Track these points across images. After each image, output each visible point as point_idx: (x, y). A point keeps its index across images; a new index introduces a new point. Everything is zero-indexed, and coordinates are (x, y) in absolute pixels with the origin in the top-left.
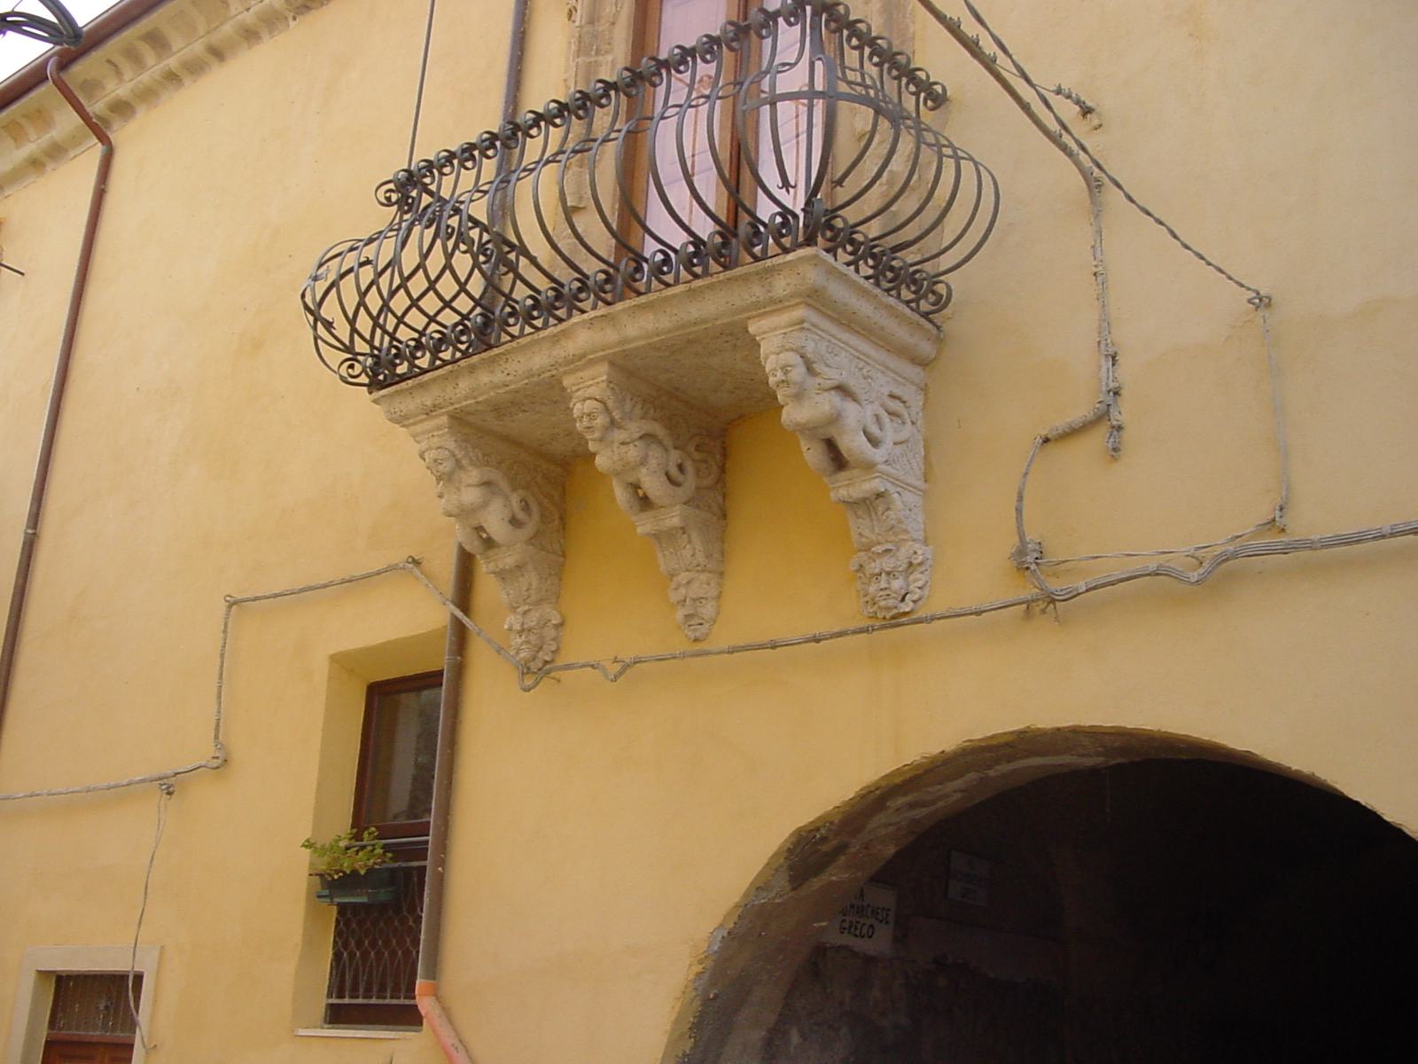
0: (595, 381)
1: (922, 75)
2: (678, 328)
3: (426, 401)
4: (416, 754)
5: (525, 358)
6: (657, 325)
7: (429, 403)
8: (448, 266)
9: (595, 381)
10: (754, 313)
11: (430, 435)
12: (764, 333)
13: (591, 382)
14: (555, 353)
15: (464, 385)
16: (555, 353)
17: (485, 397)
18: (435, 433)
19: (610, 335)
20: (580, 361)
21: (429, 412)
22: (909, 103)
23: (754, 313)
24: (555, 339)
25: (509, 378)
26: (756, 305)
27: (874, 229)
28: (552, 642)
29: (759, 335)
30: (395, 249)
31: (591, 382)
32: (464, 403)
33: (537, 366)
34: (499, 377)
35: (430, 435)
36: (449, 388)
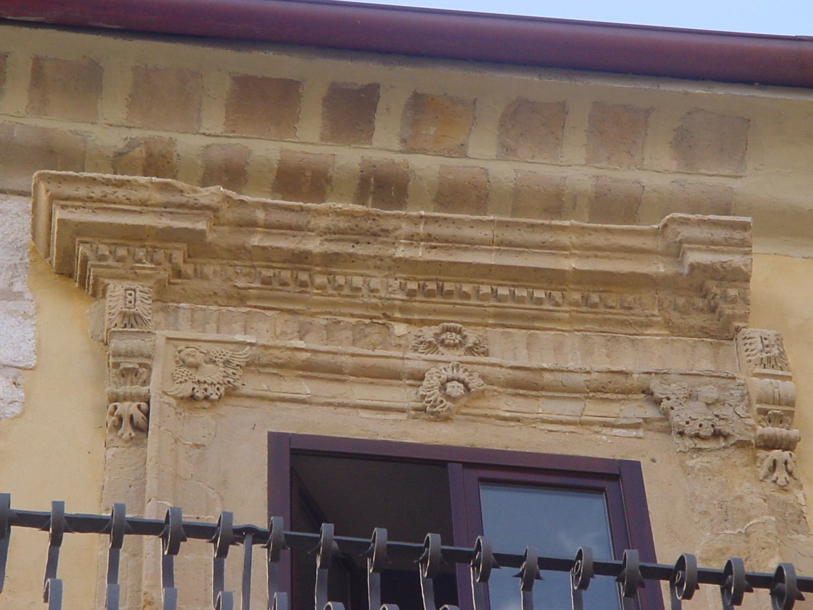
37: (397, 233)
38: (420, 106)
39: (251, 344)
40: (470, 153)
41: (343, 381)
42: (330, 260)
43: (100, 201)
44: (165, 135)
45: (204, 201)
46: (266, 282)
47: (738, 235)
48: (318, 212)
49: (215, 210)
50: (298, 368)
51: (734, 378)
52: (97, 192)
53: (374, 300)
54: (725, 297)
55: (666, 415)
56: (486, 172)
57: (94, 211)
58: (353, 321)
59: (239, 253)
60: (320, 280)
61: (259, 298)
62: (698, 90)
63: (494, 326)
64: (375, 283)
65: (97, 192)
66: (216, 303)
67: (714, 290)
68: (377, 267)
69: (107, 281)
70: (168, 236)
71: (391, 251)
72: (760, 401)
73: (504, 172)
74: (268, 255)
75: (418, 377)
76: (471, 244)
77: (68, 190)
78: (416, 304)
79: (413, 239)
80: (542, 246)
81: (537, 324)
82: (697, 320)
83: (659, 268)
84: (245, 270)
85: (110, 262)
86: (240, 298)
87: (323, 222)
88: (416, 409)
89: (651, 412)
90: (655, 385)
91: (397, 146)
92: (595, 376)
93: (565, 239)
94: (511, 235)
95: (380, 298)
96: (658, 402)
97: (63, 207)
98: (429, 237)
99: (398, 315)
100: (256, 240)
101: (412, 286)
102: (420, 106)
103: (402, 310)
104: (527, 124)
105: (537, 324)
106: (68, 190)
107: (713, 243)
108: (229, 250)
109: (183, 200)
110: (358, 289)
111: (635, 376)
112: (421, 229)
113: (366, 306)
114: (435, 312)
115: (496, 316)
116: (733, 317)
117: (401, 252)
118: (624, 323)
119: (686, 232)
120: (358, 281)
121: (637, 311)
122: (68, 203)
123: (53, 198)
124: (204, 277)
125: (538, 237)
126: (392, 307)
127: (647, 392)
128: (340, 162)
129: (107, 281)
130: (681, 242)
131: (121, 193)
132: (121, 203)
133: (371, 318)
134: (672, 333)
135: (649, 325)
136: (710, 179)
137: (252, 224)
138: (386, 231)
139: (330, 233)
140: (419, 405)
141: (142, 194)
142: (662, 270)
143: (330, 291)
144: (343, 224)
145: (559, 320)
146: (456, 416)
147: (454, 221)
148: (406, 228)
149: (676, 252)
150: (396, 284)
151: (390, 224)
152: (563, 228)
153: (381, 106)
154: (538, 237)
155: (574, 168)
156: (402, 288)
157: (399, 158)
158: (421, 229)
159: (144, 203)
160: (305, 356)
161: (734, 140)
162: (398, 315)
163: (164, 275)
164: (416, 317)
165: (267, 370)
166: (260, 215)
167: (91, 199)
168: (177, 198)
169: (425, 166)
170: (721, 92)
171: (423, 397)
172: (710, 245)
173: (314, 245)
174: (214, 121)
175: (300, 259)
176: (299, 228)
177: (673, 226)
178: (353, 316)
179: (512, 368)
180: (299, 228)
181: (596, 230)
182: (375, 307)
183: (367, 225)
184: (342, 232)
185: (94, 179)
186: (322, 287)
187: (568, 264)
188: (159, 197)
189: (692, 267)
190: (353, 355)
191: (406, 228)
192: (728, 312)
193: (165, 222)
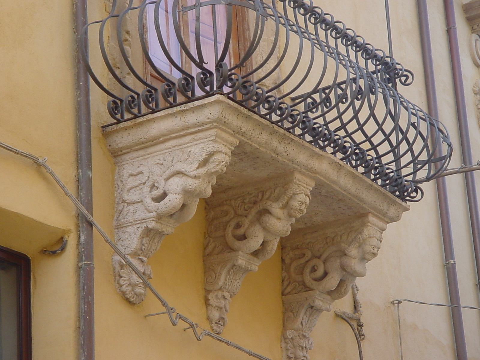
0: (307, 187)
1: (328, 18)
2: (354, 196)
3: (244, 127)
4: (78, 261)
5: (297, 153)
6: (351, 188)
7: (244, 129)
8: (372, 115)
9: (307, 187)
10: (375, 213)
11: (225, 144)
12: (373, 224)
13: (305, 186)
14: (310, 161)
15: (265, 137)
16: (310, 161)
17: (264, 150)
18: (228, 145)
19: (332, 174)
20: (310, 172)
21: (236, 132)
22: (342, 49)
23: (375, 213)
24: (313, 155)
25: (284, 154)
26: (380, 211)
27: (269, 82)
28: (289, 348)
29: (371, 224)
30: (428, 129)
31: (305, 186)
33: (299, 160)
34: (281, 148)
35: (225, 144)
36: (258, 132)
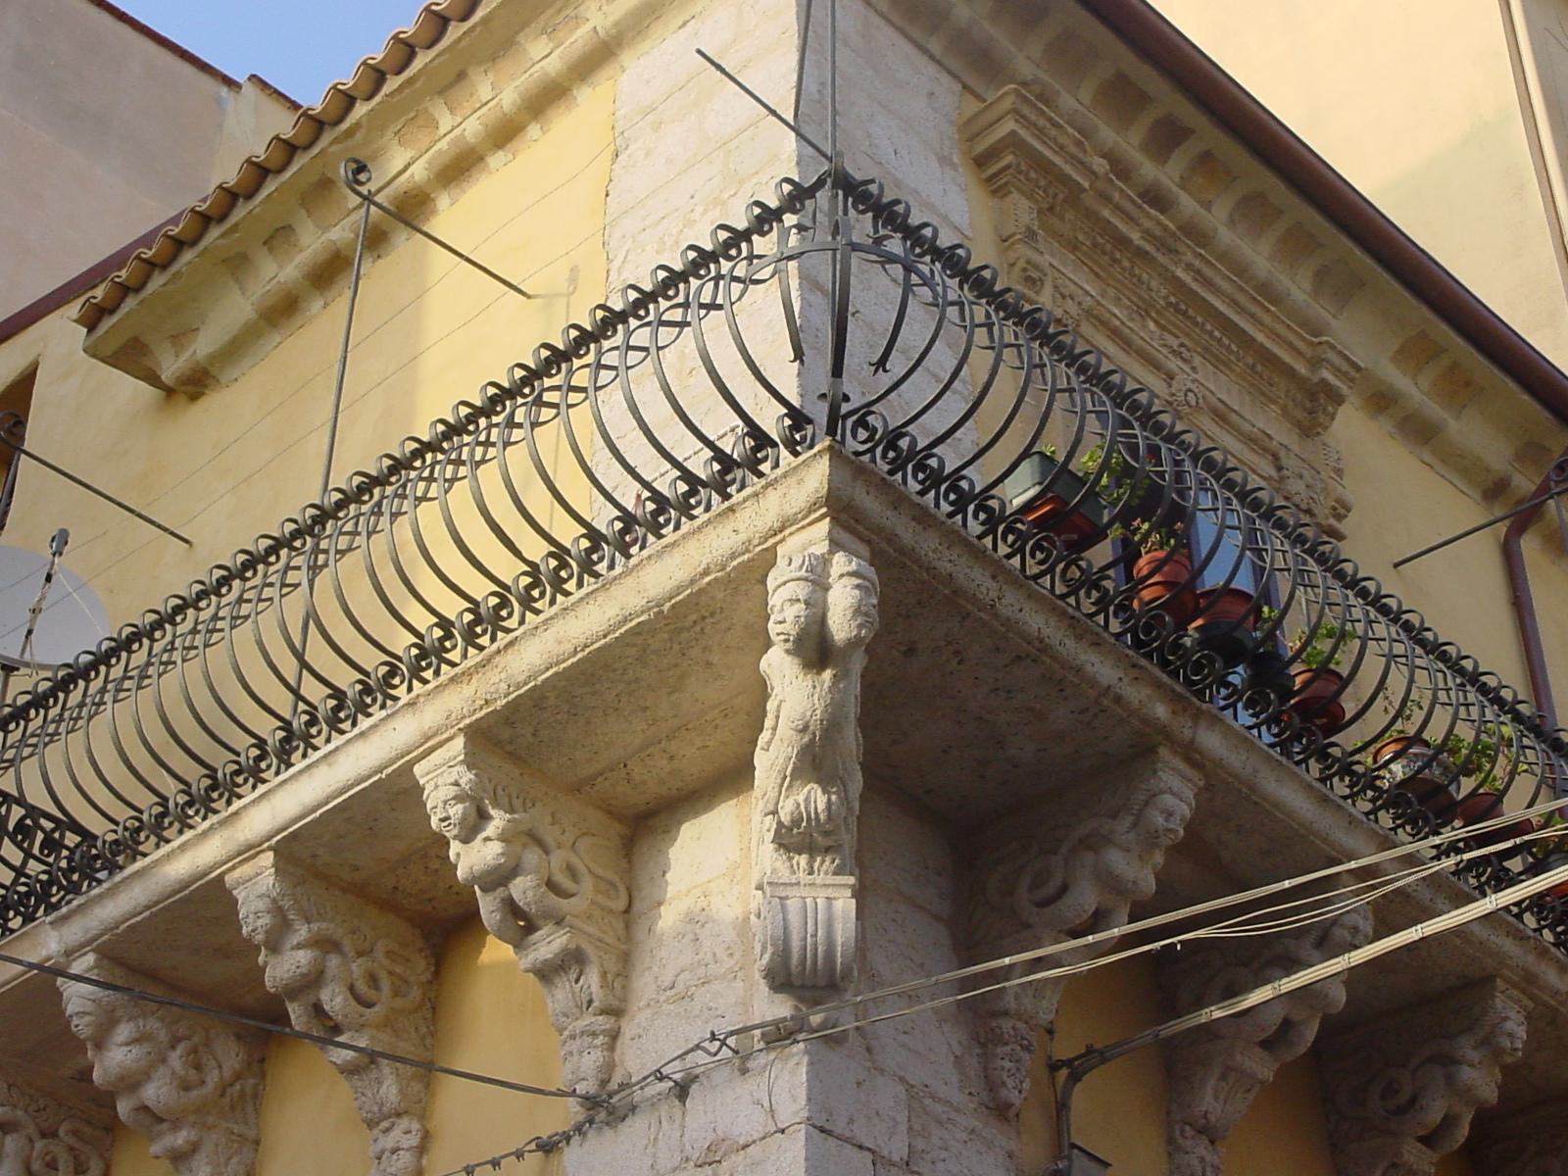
32: (1317, 842)
35: (643, 755)
37: (1184, 258)
38: (1206, 160)
39: (1092, 296)
40: (1213, 210)
41: (1128, 353)
42: (1141, 253)
43: (1038, 129)
44: (1057, 87)
45: (1095, 168)
46: (1095, 245)
47: (1353, 373)
48: (1148, 215)
49: (1097, 177)
50: (1109, 329)
51: (1319, 473)
52: (1041, 122)
53: (1146, 297)
54: (1325, 409)
55: (1282, 479)
56: (1216, 230)
57: (1033, 135)
58: (1129, 303)
59: (1091, 215)
60: (1126, 264)
61: (1085, 254)
62: (1358, 252)
63: (1199, 354)
64: (1154, 284)
65: (1041, 122)
66: (1059, 242)
67: (1322, 401)
68: (1160, 275)
69: (1012, 189)
70: (1065, 179)
71: (1174, 268)
72: (1337, 501)
73: (1226, 236)
74: (1106, 227)
75: (1170, 377)
76: (1217, 291)
77: (1026, 110)
78: (1167, 314)
79: (1189, 267)
80: (1252, 316)
81: (1222, 368)
82: (1300, 414)
83: (1302, 369)
84: (1086, 230)
85: (1022, 178)
86: (1073, 246)
87: (1148, 224)
88: (1167, 402)
89: (1273, 473)
90: (1282, 453)
91: (1177, 180)
92: (1255, 430)
93: (1267, 319)
94: (1242, 299)
95: (1151, 297)
96: (1280, 469)
97: (1017, 121)
98: (1198, 272)
99: (1154, 315)
100: (1106, 213)
101: (1173, 299)
102: (1206, 160)
103: (1157, 312)
104: (1254, 211)
105: (1222, 368)
106: (1026, 110)
107: (1339, 370)
108: (1087, 209)
109: (1085, 159)
110: (1143, 283)
111: (1274, 442)
112: (1197, 263)
113: (1140, 298)
114: (1174, 325)
115: (1206, 349)
116: (1320, 425)
117: (1180, 273)
118: (1263, 394)
119: (1331, 355)
120: (1145, 276)
121: (1274, 389)
122: (1022, 120)
123: (1015, 111)
124: (1062, 218)
125: (1254, 309)
126: (1154, 307)
127: (1276, 457)
128: (1143, 171)
129: (1012, 189)
130: (1323, 360)
131: (1054, 132)
132: (1050, 139)
133: (1138, 307)
134: (1283, 416)
135: (1274, 402)
136: (1320, 310)
137: (1108, 199)
138: (1177, 252)
139: (1147, 234)
140: (1170, 399)
141: (1063, 140)
142: (1303, 371)
143: (1127, 275)
144: (1158, 232)
145: (1232, 370)
146: (1185, 420)
147: (1216, 268)
148: (1189, 257)
149: (1315, 363)
150: (1164, 292)
151: (1182, 248)
152: (1268, 310)
153: (1184, 145)
154: (1254, 309)
155: (1260, 255)
156: (1166, 298)
157: (1175, 189)
158: (1197, 263)
159: (1062, 148)
160: (1118, 323)
161: (1341, 288)
162: (1154, 315)
163: (1045, 205)
164: (1163, 322)
165: (1093, 320)
166: (1117, 196)
167: (1035, 125)
168: (1081, 156)
169: (1187, 203)
170: (1369, 261)
171: (1173, 395)
172: (1337, 371)
173: (1136, 237)
174: (1086, 93)
175: (1122, 242)
176: (1132, 219)
177: (1325, 346)
178: (1129, 299)
179: (1219, 399)
180: (1132, 219)
181: (1283, 322)
182: (1144, 300)
183: (1170, 241)
184: (1155, 238)
185: (1044, 112)
186: (1123, 269)
187: (1260, 337)
188: (1072, 149)
189: (1323, 380)
190: (1142, 338)
191: (1189, 257)
192: (1321, 420)
193: (1068, 169)
